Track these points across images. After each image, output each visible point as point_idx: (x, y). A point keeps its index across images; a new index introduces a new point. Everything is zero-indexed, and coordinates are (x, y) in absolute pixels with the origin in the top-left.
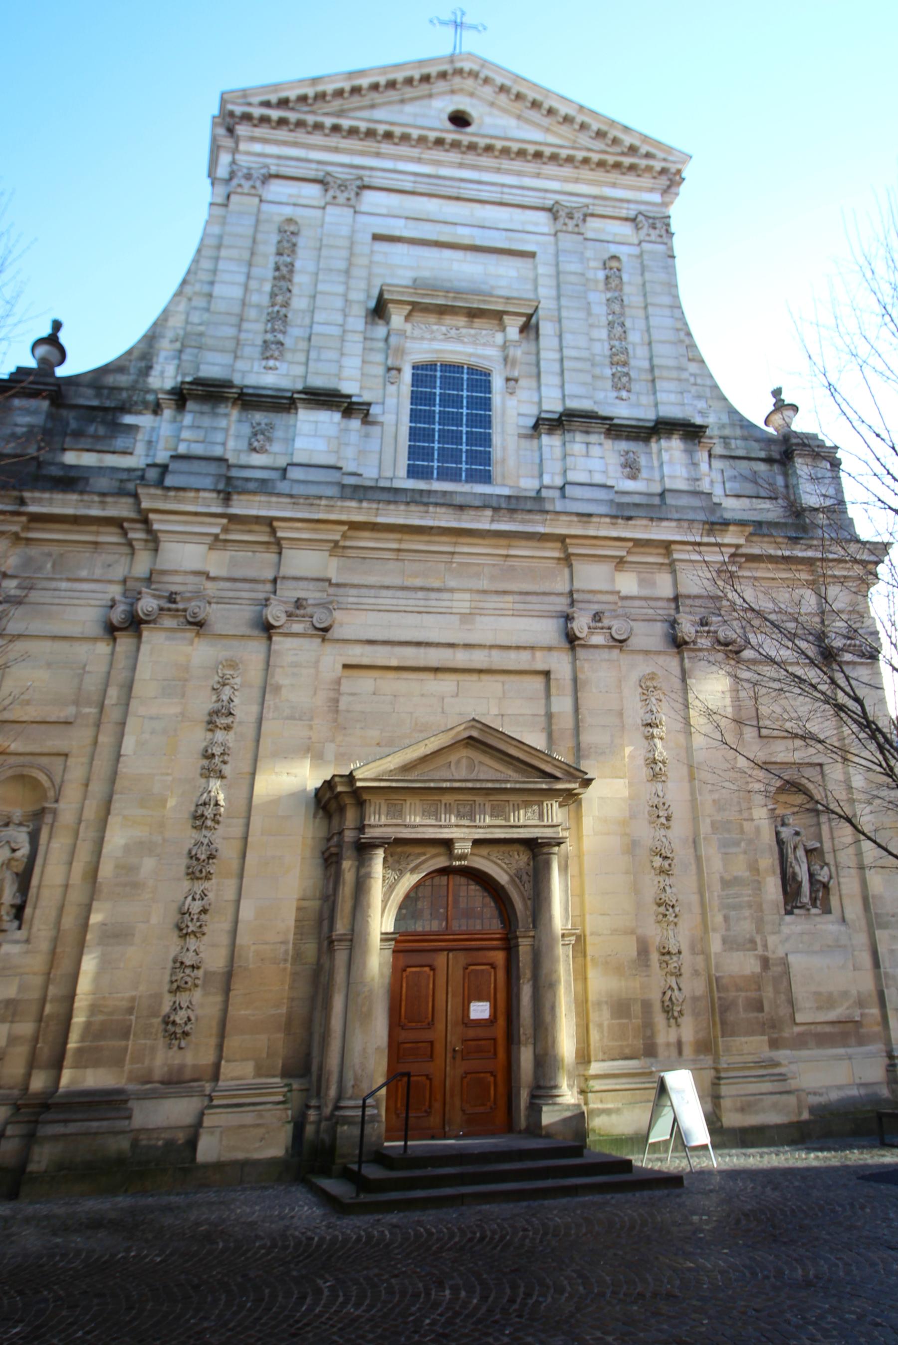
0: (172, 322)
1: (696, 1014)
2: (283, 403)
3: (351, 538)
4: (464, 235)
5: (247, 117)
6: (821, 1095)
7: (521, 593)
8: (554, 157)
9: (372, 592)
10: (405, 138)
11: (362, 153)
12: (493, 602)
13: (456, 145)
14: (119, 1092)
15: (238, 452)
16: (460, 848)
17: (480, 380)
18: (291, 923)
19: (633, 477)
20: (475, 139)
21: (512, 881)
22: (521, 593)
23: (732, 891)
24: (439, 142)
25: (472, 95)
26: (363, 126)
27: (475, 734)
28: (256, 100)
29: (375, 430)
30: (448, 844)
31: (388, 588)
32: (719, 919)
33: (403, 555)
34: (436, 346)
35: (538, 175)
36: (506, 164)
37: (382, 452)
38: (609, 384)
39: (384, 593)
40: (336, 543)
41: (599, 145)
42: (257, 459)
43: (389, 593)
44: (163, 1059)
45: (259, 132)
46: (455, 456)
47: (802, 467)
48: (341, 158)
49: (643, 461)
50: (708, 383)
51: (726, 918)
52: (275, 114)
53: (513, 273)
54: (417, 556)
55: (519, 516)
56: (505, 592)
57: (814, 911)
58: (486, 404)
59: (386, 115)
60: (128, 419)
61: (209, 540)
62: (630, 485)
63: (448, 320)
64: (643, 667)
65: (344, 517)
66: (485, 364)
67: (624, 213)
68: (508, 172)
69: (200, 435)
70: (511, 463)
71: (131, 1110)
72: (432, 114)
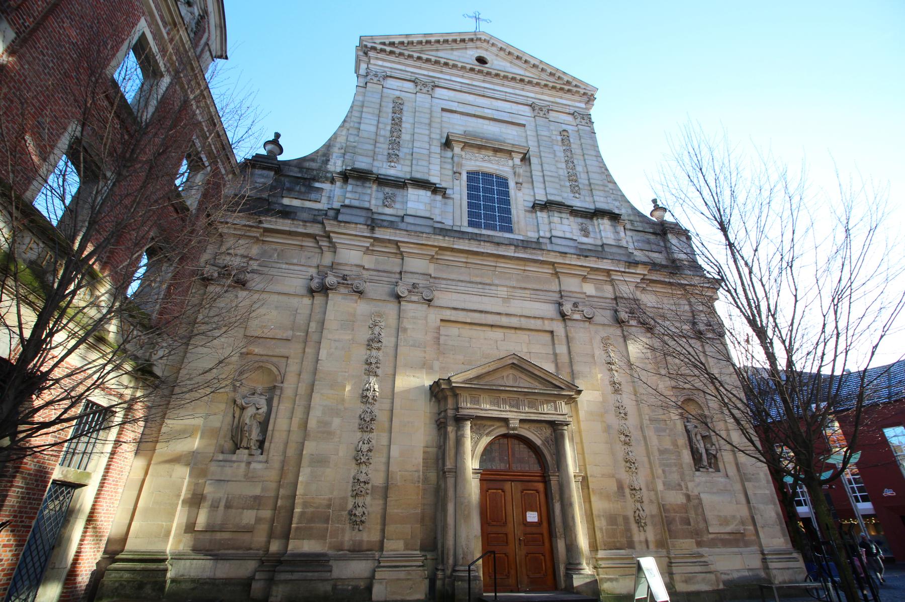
1: (654, 525)
9: (454, 283)
10: (455, 66)
11: (433, 71)
12: (519, 293)
13: (480, 72)
19: (587, 236)
21: (544, 444)
27: (515, 362)
28: (378, 41)
30: (506, 421)
33: (470, 265)
35: (523, 90)
36: (506, 83)
39: (460, 284)
40: (433, 256)
41: (551, 79)
43: (463, 284)
44: (348, 537)
45: (380, 56)
48: (424, 72)
51: (664, 471)
52: (388, 49)
54: (473, 266)
55: (529, 251)
56: (525, 289)
57: (711, 470)
59: (444, 55)
60: (317, 185)
61: (364, 249)
63: (483, 152)
65: (436, 244)
67: (567, 111)
68: (507, 86)
72: (469, 56)
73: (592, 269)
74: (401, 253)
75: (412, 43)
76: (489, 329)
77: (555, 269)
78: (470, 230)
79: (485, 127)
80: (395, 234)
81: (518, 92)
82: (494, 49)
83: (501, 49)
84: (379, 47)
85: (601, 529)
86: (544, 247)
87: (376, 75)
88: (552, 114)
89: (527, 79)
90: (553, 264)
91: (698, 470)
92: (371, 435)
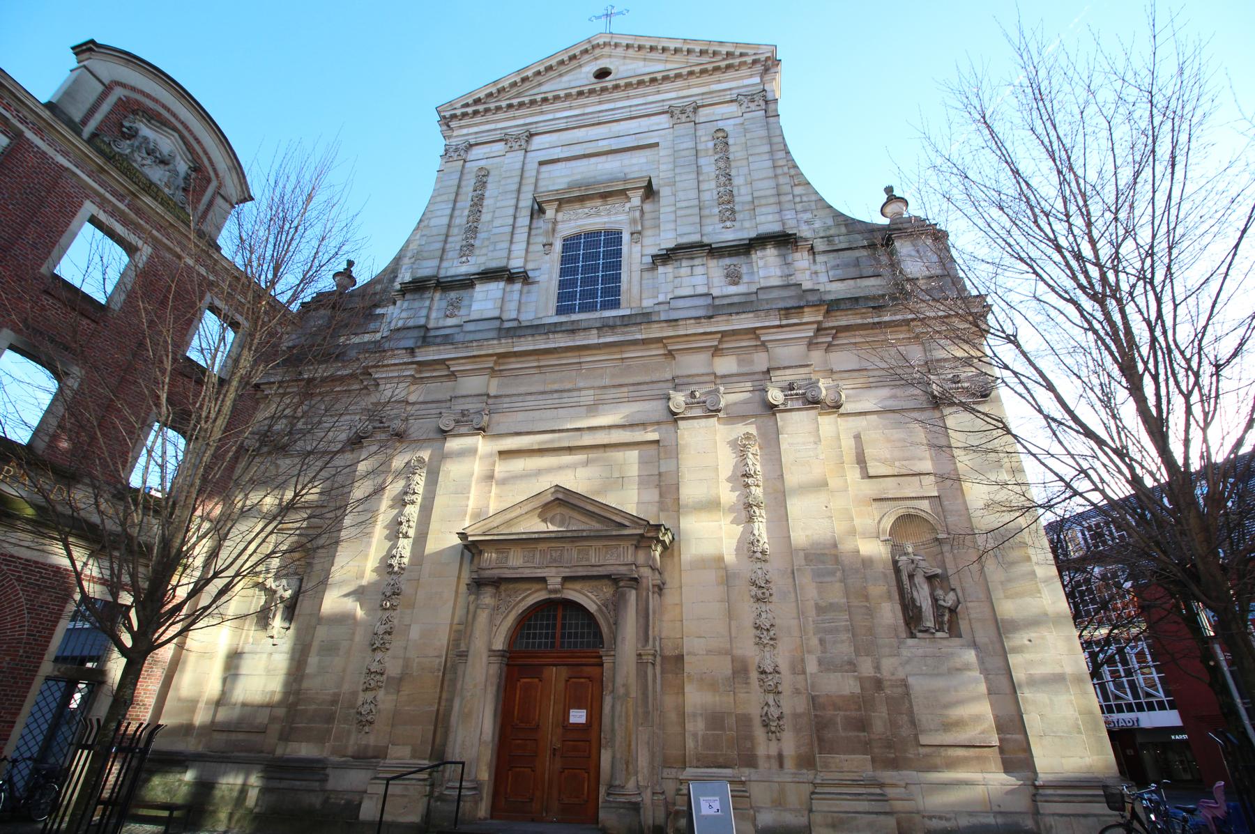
0: (411, 247)
1: (797, 730)
2: (467, 283)
3: (503, 364)
4: (604, 145)
5: (454, 117)
6: (947, 819)
7: (633, 384)
8: (665, 78)
9: (521, 398)
10: (556, 98)
11: (532, 115)
12: (612, 394)
13: (604, 90)
14: (318, 761)
15: (437, 319)
16: (554, 582)
17: (614, 238)
18: (445, 642)
19: (735, 283)
21: (600, 609)
22: (633, 384)
23: (828, 616)
24: (592, 92)
25: (610, 56)
27: (560, 496)
29: (534, 288)
30: (543, 580)
31: (531, 394)
32: (814, 642)
33: (543, 370)
34: (580, 222)
35: (658, 92)
36: (632, 92)
37: (540, 303)
38: (717, 219)
39: (529, 398)
40: (492, 368)
41: (705, 59)
42: (450, 322)
43: (533, 398)
44: (355, 741)
45: (463, 122)
46: (593, 294)
47: (903, 248)
48: (513, 123)
49: (744, 269)
50: (813, 198)
51: (822, 641)
52: (470, 110)
53: (643, 160)
54: (549, 370)
55: (619, 330)
56: (621, 386)
57: (939, 634)
58: (618, 253)
59: (551, 87)
60: (379, 311)
61: (805, 342)
62: (733, 289)
63: (589, 204)
64: (741, 429)
65: (491, 352)
66: (616, 226)
67: (728, 98)
68: (635, 97)
69: (411, 313)
70: (635, 290)
71: (328, 775)
72: (584, 75)
73: (724, 334)
74: (763, 344)
75: (504, 89)
76: (602, 450)
77: (665, 346)
78: (563, 319)
79: (600, 166)
80: (439, 352)
81: (651, 99)
82: (620, 51)
83: (628, 46)
84: (458, 112)
85: (695, 735)
86: (654, 318)
87: (683, 112)
88: (702, 111)
89: (659, 76)
90: (659, 340)
91: (913, 636)
92: (394, 614)
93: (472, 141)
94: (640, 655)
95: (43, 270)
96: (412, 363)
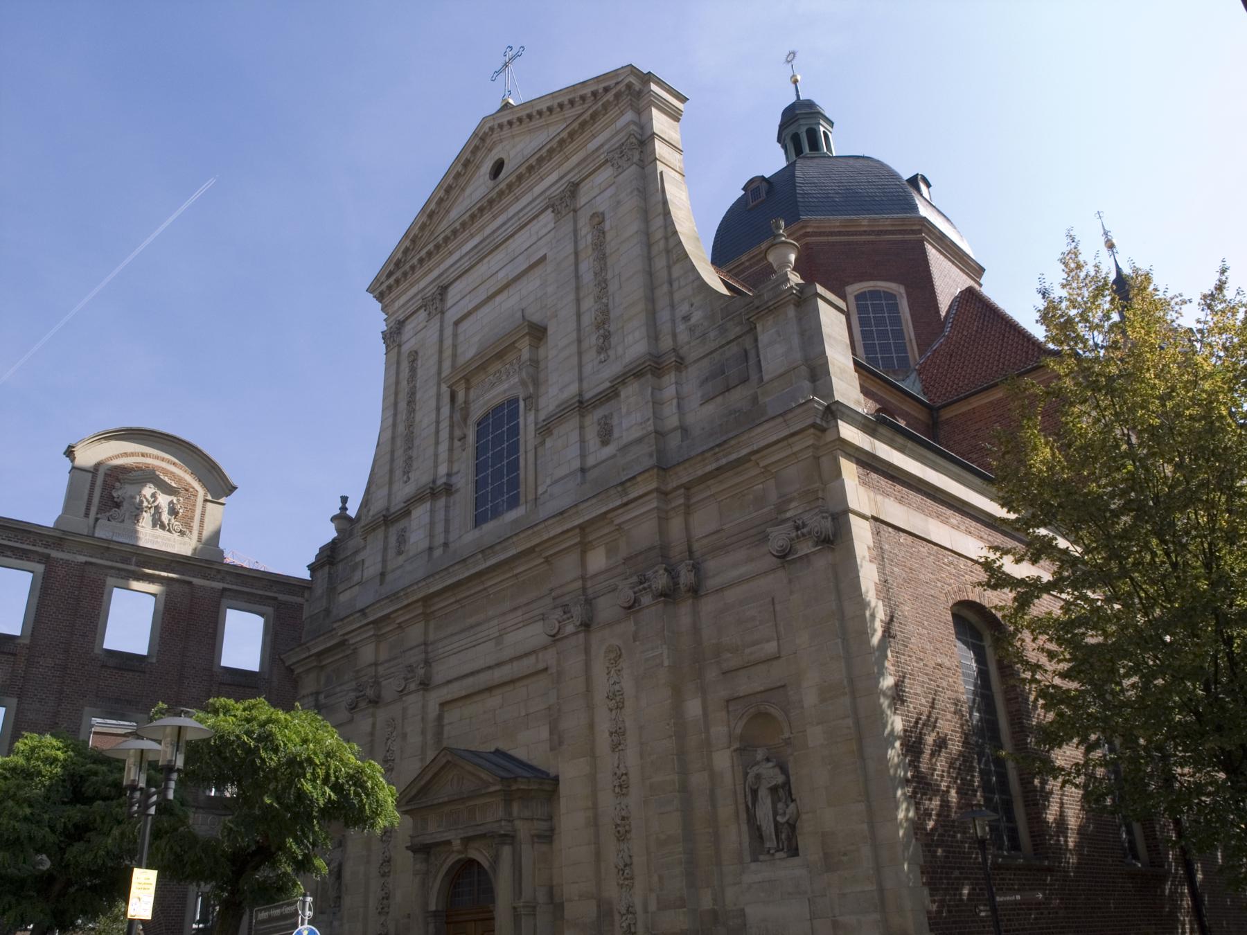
20: (508, 181)
26: (448, 232)
28: (384, 278)
34: (488, 396)
52: (398, 274)
59: (443, 227)
63: (492, 369)
65: (415, 598)
93: (401, 317)
94: (515, 908)
95: (96, 651)
96: (367, 624)
